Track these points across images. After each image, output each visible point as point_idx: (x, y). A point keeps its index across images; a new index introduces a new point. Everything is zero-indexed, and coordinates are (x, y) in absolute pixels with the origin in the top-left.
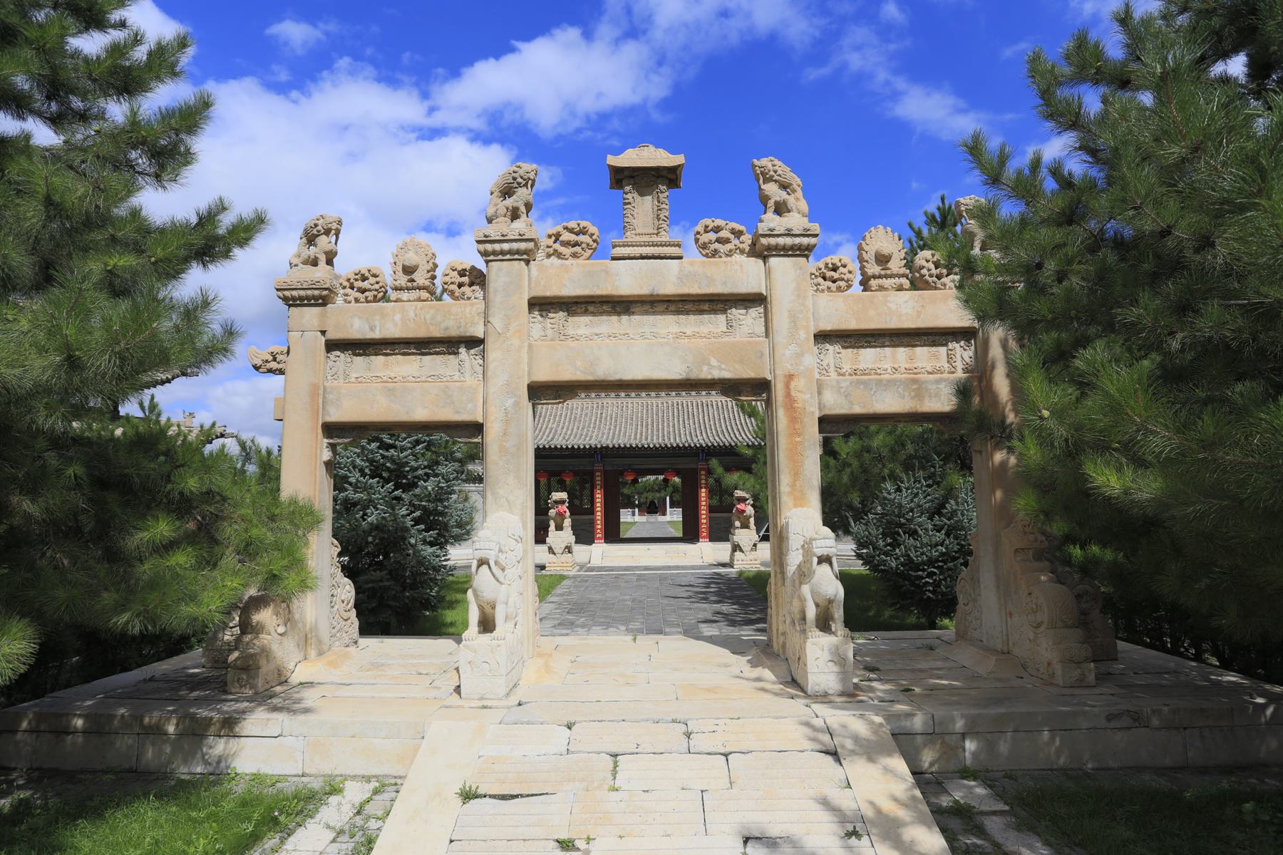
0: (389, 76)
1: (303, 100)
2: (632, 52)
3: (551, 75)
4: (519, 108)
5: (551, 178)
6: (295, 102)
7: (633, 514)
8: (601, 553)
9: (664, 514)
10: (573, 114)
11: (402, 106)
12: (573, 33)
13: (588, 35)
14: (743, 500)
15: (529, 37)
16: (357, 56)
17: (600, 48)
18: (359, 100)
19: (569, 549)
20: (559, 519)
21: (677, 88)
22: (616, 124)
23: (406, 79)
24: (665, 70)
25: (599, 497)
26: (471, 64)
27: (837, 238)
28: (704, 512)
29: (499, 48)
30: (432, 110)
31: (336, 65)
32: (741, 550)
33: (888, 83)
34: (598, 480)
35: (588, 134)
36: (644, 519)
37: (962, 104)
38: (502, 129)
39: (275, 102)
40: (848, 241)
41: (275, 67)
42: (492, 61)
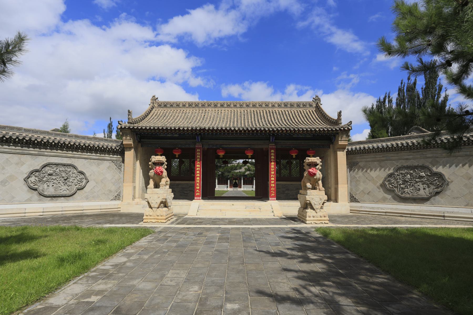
0: (141, 22)
1: (107, 29)
2: (233, 14)
3: (201, 23)
4: (190, 35)
5: (201, 62)
6: (104, 30)
7: (227, 187)
8: (198, 208)
9: (240, 187)
10: (210, 38)
11: (146, 33)
12: (211, 7)
13: (217, 8)
14: (315, 165)
15: (194, 8)
16: (129, 13)
17: (221, 12)
18: (130, 30)
19: (164, 204)
20: (157, 178)
21: (249, 29)
22: (225, 42)
23: (146, 22)
24: (245, 22)
25: (198, 166)
26: (172, 18)
27: (306, 88)
28: (272, 178)
29: (183, 13)
30: (158, 34)
31: (120, 16)
32: (312, 208)
33: (329, 29)
34: (199, 155)
35: (216, 45)
36: (232, 189)
37: (356, 38)
38: (185, 43)
39: (96, 30)
40: (311, 89)
41: (97, 16)
42: (180, 17)
